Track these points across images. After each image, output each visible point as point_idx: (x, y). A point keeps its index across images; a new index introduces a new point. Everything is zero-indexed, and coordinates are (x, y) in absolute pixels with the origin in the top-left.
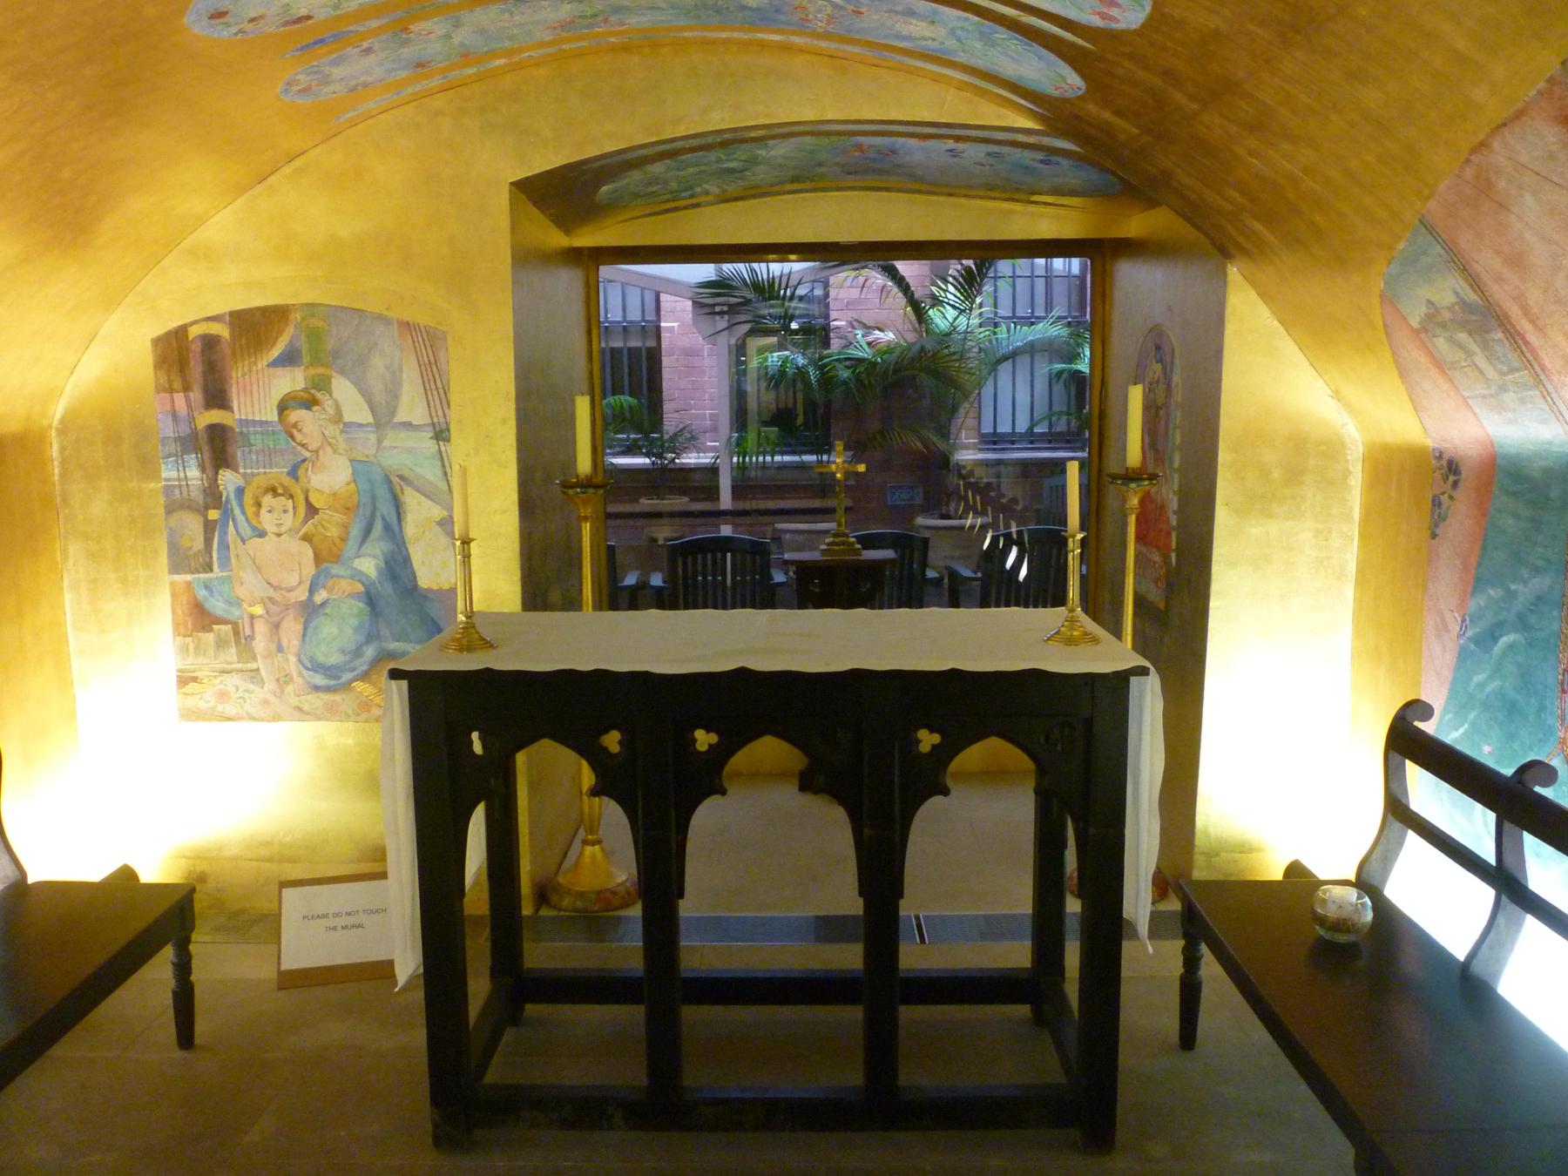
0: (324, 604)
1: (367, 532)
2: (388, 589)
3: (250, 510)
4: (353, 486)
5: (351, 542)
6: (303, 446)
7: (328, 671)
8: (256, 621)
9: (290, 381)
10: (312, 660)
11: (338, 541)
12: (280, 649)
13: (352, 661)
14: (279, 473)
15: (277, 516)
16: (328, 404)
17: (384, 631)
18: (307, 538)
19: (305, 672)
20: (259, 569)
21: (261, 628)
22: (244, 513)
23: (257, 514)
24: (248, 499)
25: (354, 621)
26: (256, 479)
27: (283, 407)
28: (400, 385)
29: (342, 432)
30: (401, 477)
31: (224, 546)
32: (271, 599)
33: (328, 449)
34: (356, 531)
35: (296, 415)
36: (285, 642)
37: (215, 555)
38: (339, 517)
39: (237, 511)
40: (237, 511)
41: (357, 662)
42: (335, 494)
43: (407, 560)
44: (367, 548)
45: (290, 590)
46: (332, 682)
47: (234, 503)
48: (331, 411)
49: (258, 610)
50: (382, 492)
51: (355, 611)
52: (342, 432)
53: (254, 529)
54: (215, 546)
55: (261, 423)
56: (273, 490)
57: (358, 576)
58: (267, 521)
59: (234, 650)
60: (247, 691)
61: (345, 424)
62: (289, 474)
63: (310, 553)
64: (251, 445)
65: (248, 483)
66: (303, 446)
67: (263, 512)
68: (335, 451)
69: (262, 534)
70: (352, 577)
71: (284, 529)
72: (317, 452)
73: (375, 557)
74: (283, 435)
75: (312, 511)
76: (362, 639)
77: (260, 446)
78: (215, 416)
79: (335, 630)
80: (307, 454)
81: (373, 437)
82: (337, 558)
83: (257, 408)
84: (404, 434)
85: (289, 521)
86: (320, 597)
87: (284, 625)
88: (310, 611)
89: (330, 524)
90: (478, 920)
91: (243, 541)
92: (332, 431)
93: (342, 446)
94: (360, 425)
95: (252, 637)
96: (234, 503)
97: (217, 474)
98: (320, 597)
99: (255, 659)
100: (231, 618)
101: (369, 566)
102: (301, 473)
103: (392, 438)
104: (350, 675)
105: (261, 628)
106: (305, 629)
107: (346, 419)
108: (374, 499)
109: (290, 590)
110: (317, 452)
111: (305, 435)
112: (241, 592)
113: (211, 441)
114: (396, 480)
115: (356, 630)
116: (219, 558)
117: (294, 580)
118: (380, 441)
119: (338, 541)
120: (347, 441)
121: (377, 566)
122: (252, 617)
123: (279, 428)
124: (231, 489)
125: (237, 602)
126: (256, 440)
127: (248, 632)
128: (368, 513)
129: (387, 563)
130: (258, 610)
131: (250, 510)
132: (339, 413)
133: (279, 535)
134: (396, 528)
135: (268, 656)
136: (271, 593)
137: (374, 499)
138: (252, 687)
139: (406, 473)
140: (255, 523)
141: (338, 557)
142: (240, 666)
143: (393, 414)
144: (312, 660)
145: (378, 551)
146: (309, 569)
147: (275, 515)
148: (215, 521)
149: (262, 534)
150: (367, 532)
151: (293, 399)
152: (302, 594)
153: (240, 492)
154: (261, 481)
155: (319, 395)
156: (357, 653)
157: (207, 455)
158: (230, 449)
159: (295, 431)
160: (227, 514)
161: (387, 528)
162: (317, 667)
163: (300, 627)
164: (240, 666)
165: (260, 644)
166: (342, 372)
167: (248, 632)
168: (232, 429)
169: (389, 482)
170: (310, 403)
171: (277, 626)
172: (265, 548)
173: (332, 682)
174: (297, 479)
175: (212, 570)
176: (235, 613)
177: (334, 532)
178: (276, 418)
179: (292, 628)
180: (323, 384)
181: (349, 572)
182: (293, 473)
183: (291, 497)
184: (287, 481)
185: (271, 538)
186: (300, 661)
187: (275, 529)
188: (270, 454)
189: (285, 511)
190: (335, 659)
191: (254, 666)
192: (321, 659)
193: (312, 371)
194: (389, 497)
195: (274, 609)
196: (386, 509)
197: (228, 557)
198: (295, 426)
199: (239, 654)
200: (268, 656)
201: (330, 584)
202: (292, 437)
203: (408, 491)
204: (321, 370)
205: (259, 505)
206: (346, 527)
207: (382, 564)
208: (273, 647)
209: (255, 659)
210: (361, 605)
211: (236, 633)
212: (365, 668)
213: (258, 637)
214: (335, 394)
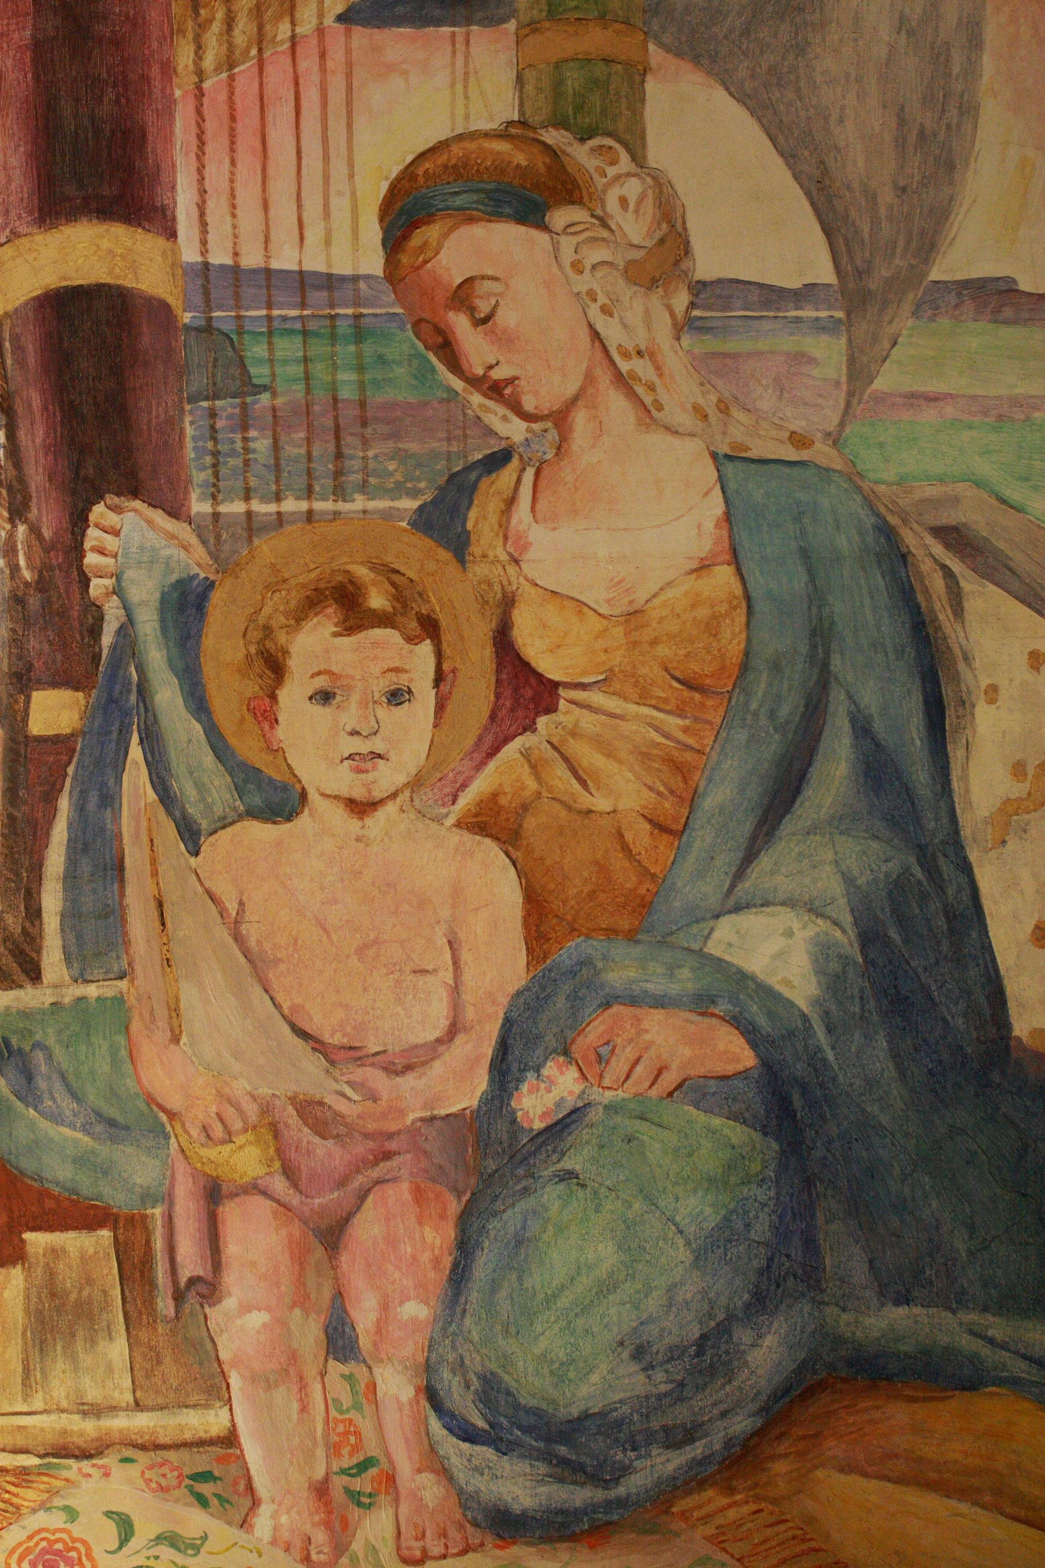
0: (563, 1126)
1: (782, 794)
2: (868, 1066)
3: (229, 692)
4: (725, 573)
5: (701, 838)
6: (495, 390)
7: (556, 1439)
8: (231, 1213)
9: (444, 91)
10: (490, 1390)
11: (640, 835)
12: (340, 1341)
13: (679, 1393)
14: (382, 509)
15: (356, 716)
16: (622, 192)
17: (846, 1257)
18: (494, 822)
19: (453, 1449)
20: (257, 964)
21: (255, 1240)
22: (199, 705)
23: (264, 713)
24: (223, 643)
25: (698, 1209)
26: (266, 547)
27: (408, 210)
28: (969, 110)
29: (685, 325)
30: (953, 537)
31: (100, 861)
32: (308, 1109)
33: (616, 403)
34: (728, 790)
35: (460, 250)
36: (364, 1316)
37: (52, 900)
38: (642, 722)
39: (168, 696)
40: (168, 696)
41: (702, 1403)
42: (634, 617)
43: (968, 917)
44: (777, 868)
45: (405, 1064)
46: (580, 1496)
47: (156, 656)
48: (636, 229)
49: (246, 1160)
50: (862, 607)
51: (709, 1160)
52: (685, 325)
53: (244, 776)
54: (55, 859)
55: (303, 282)
56: (348, 604)
57: (728, 996)
58: (309, 742)
59: (117, 1349)
60: (171, 1540)
61: (699, 288)
62: (424, 521)
63: (506, 890)
64: (250, 387)
65: (225, 565)
66: (495, 390)
67: (293, 696)
68: (648, 414)
69: (281, 802)
70: (702, 1003)
71: (387, 778)
72: (560, 418)
73: (814, 909)
74: (406, 342)
75: (525, 692)
76: (729, 1288)
77: (290, 394)
78: (85, 252)
79: (605, 1254)
80: (515, 430)
81: (829, 354)
82: (639, 913)
83: (284, 213)
84: (976, 336)
85: (410, 737)
86: (535, 1104)
87: (367, 1228)
88: (492, 1163)
89: (609, 760)
90: (143, 603)
91: (191, 836)
92: (642, 320)
93: (681, 390)
94: (772, 296)
95: (207, 1288)
96: (156, 656)
97: (79, 521)
98: (535, 1104)
99: (217, 1390)
100: (118, 1199)
101: (781, 950)
102: (481, 518)
103: (917, 355)
104: (665, 1463)
105: (255, 1240)
106: (465, 1248)
107: (707, 264)
108: (821, 636)
109: (405, 1064)
110: (560, 418)
111: (506, 340)
112: (166, 1074)
113: (59, 366)
114: (927, 551)
115: (708, 1249)
116: (71, 916)
117: (427, 1019)
118: (858, 373)
119: (640, 835)
120: (712, 366)
121: (822, 953)
122: (214, 1193)
123: (389, 305)
124: (145, 591)
125: (147, 1122)
126: (277, 363)
127: (191, 1260)
128: (789, 708)
129: (869, 937)
130: (246, 1160)
131: (229, 692)
132: (673, 244)
133: (361, 808)
134: (921, 776)
135: (289, 1369)
136: (310, 1075)
137: (821, 636)
138: (195, 1521)
139: (973, 515)
140: (248, 748)
141: (644, 906)
142: (143, 1422)
143: (928, 247)
144: (490, 1390)
145: (828, 884)
146: (500, 967)
147: (351, 716)
148: (62, 745)
149: (281, 802)
150: (782, 794)
151: (460, 172)
152: (458, 1085)
153: (187, 605)
154: (293, 556)
155: (581, 155)
156: (709, 1354)
157: (122, 672)
158: (151, 408)
159: (460, 323)
160: (120, 711)
161: (877, 769)
162: (504, 1421)
163: (437, 1238)
164: (143, 1422)
165: (243, 1323)
166: (699, 51)
167: (191, 1260)
168: (161, 310)
169: (891, 554)
170: (532, 194)
171: (332, 1234)
172: (285, 875)
173: (580, 1496)
174: (459, 547)
175: (34, 975)
176: (139, 1169)
177: (624, 792)
178: (372, 261)
179: (399, 1249)
180: (599, 105)
181: (686, 981)
182: (445, 520)
183: (430, 628)
184: (418, 557)
185: (322, 819)
186: (432, 1396)
187: (345, 781)
188: (339, 432)
189: (396, 697)
190: (602, 1383)
191: (212, 1421)
192: (531, 1383)
193: (559, 43)
194: (891, 628)
195: (324, 1154)
196: (875, 687)
197: (114, 915)
198: (462, 297)
199: (144, 1366)
200: (289, 1369)
201: (594, 1032)
202: (447, 348)
203: (984, 599)
204: (594, 40)
205: (274, 666)
206: (681, 775)
207: (846, 941)
208: (309, 1334)
209: (217, 1390)
210: (737, 1133)
211: (135, 1267)
212: (742, 1424)
213: (238, 1285)
214: (656, 154)
